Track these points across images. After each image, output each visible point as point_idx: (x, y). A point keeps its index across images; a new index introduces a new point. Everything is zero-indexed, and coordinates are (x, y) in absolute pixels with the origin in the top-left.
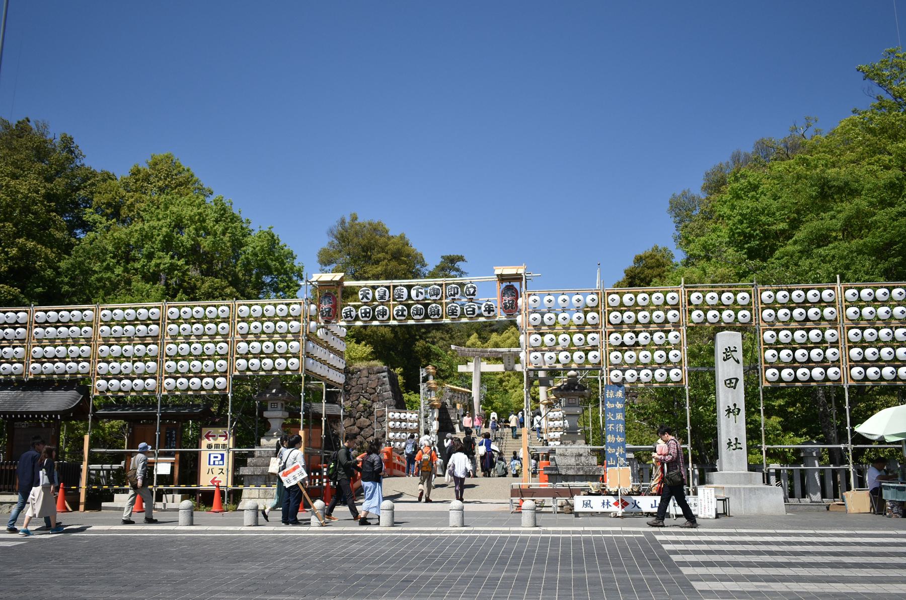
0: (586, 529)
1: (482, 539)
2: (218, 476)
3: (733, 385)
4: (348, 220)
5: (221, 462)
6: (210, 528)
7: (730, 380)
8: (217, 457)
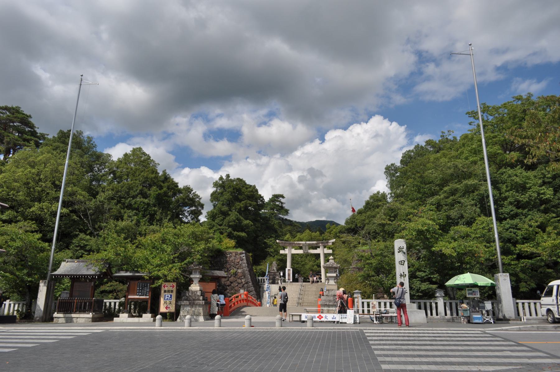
0: (335, 328)
1: (289, 332)
2: (169, 305)
3: (403, 264)
4: (224, 177)
5: (170, 299)
6: (170, 328)
7: (401, 261)
8: (168, 296)
